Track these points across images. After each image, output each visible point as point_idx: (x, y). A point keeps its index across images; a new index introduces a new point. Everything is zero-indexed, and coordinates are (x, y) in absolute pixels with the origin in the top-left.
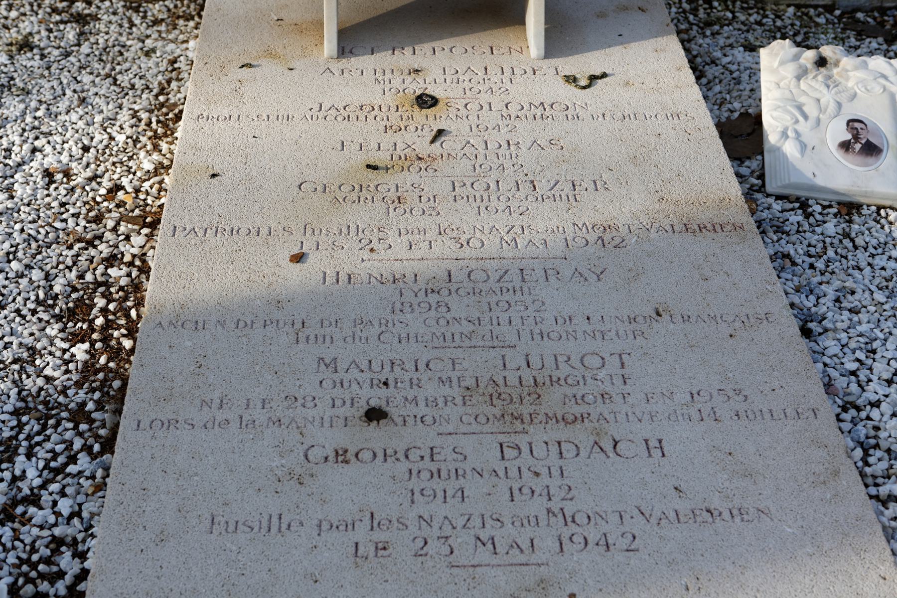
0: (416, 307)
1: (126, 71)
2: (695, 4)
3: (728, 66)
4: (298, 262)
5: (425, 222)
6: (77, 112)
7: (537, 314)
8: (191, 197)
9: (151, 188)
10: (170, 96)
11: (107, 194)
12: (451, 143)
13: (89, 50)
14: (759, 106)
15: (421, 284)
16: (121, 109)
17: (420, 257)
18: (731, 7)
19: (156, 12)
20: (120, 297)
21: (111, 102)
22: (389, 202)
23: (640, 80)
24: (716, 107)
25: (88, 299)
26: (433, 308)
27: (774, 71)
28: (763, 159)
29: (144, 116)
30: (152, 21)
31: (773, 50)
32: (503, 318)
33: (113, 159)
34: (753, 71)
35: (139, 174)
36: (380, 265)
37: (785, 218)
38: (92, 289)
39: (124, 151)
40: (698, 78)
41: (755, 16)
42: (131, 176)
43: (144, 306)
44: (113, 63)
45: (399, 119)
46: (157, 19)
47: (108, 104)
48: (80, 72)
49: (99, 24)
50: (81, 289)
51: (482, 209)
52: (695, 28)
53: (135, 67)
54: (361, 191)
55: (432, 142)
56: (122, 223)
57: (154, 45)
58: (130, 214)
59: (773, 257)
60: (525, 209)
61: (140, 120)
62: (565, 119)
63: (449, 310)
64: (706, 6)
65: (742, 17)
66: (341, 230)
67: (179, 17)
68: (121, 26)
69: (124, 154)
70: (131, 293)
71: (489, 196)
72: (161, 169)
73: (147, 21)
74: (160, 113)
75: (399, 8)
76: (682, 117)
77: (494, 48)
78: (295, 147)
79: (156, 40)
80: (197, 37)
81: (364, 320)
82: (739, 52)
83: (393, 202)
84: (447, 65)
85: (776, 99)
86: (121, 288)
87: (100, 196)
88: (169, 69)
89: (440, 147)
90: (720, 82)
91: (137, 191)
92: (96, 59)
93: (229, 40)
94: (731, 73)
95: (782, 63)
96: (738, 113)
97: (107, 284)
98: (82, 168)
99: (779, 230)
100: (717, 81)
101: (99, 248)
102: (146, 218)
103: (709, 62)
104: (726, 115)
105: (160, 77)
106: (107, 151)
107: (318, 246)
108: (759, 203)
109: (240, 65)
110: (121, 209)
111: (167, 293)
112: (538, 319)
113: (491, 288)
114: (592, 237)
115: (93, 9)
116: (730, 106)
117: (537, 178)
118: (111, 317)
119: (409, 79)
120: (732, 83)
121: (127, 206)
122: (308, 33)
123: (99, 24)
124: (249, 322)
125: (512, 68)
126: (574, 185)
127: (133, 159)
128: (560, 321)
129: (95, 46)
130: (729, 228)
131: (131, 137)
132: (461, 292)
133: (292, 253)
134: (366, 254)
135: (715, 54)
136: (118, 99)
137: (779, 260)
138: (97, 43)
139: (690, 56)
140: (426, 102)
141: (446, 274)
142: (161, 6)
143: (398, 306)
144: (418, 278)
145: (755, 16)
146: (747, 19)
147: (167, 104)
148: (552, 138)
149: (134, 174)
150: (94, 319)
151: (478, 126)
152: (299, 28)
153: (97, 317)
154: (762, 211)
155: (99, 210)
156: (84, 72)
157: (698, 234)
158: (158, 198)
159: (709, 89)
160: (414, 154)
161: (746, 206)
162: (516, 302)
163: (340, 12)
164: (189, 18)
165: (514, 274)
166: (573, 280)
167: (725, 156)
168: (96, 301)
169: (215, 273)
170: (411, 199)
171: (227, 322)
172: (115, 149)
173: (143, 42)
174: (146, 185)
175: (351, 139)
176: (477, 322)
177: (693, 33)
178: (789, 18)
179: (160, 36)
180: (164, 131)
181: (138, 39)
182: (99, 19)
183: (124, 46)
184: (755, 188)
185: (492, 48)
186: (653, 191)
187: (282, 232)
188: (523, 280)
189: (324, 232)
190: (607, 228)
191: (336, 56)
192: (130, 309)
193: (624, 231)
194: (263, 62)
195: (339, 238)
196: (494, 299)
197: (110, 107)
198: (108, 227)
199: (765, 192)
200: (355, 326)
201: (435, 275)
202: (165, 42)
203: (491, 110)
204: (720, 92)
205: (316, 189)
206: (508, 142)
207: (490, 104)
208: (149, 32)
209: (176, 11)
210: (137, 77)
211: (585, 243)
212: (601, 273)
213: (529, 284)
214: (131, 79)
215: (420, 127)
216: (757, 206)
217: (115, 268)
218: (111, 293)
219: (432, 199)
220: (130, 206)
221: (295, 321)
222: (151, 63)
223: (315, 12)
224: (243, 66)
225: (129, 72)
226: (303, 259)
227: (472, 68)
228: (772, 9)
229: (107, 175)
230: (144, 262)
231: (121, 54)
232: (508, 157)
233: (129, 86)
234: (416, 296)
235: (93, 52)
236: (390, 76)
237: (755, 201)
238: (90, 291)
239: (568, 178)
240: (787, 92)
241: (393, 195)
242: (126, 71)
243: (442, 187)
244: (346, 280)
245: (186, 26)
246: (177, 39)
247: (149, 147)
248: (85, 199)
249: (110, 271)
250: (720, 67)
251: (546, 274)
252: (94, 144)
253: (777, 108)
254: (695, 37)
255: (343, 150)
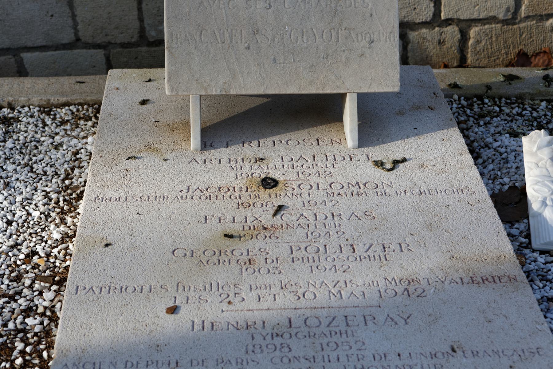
0: (264, 348)
1: (40, 161)
2: (471, 101)
3: (498, 149)
4: (172, 313)
5: (270, 279)
6: (3, 194)
7: (359, 352)
8: (90, 262)
9: (59, 253)
10: (73, 180)
11: (25, 258)
12: (288, 216)
13: (13, 145)
14: (523, 180)
15: (269, 330)
16: (36, 191)
17: (267, 308)
18: (498, 103)
19: (63, 115)
20: (35, 342)
21: (29, 186)
22: (242, 263)
23: (432, 163)
24: (491, 181)
25: (10, 343)
26: (278, 349)
27: (533, 154)
28: (529, 222)
29: (54, 196)
30: (60, 122)
31: (532, 139)
32: (333, 355)
33: (30, 231)
34: (517, 152)
35: (49, 242)
36: (236, 314)
37: (548, 269)
38: (13, 335)
39: (38, 224)
40: (475, 158)
41: (517, 109)
42: (43, 244)
43: (53, 348)
44: (30, 154)
45: (248, 198)
46: (63, 120)
47: (26, 187)
48: (5, 162)
49: (20, 125)
50: (5, 335)
51: (314, 268)
52: (471, 119)
53: (47, 158)
54: (220, 255)
55: (275, 215)
56: (36, 282)
57: (61, 140)
58: (43, 274)
59: (541, 301)
60: (347, 267)
61: (50, 200)
62: (376, 195)
63: (290, 350)
64: (479, 102)
65: (507, 111)
66: (205, 287)
67: (80, 118)
68: (36, 126)
69: (38, 226)
70: (43, 338)
71: (319, 258)
72: (66, 238)
73: (56, 122)
74: (66, 194)
75: (247, 111)
76: (465, 191)
77: (320, 141)
78: (169, 221)
79: (63, 136)
80: (94, 133)
81: (224, 359)
82: (506, 138)
83: (245, 263)
84: (285, 154)
85: (536, 176)
86: (36, 334)
87: (20, 260)
88: (73, 159)
89: (280, 219)
90: (493, 161)
91: (48, 255)
92: (17, 152)
93: (119, 138)
94: (501, 154)
95: (539, 148)
96: (508, 186)
97: (25, 331)
98: (6, 238)
99: (543, 278)
100: (490, 160)
101: (19, 301)
102: (55, 277)
103: (484, 146)
104: (498, 187)
105: (66, 166)
106: (25, 224)
107: (188, 300)
108: (527, 257)
109: (127, 158)
110: (36, 271)
111: (71, 340)
112: (360, 357)
113: (323, 332)
114: (400, 289)
115: (16, 113)
116: (501, 180)
117: (356, 242)
118: (28, 358)
119: (255, 166)
120: (501, 162)
121: (41, 268)
122: (178, 131)
123: (20, 125)
124: (135, 363)
125: (334, 156)
126: (384, 248)
127: (45, 230)
128: (377, 357)
129: (16, 142)
130: (505, 279)
131: (44, 213)
132: (299, 335)
133: (168, 306)
134: (225, 306)
135: (487, 139)
136: (34, 183)
137: (545, 303)
138: (18, 140)
139: (469, 142)
140: (269, 184)
141: (287, 321)
142: (67, 110)
143: (250, 348)
144: (265, 324)
145: (517, 109)
146: (511, 112)
147: (71, 187)
148: (366, 210)
149: (46, 242)
150: (15, 360)
151: (309, 202)
152: (171, 128)
153: (17, 358)
154: (530, 264)
155: (19, 271)
156: (8, 162)
157: (482, 285)
158: (64, 261)
159: (485, 167)
160: (260, 225)
161: (518, 261)
162: (342, 343)
163: (202, 115)
164: (87, 119)
165: (340, 320)
166: (386, 324)
167: (500, 222)
168: (16, 344)
169: (108, 323)
170: (259, 261)
171: (118, 363)
172: (32, 222)
173: (53, 138)
174: (55, 251)
175: (212, 214)
176: (312, 360)
177: (471, 123)
178: (543, 110)
179: (66, 133)
180: (69, 208)
181: (50, 136)
182: (20, 121)
183: (38, 142)
184: (523, 245)
185: (318, 141)
186: (445, 251)
187: (160, 289)
188: (348, 325)
189: (192, 288)
190: (411, 281)
191: (199, 147)
192: (43, 351)
193: (424, 283)
194: (144, 154)
195: (204, 294)
196: (325, 341)
197: (28, 189)
198: (26, 285)
199: (531, 248)
200: (217, 365)
201: (279, 322)
202: (70, 138)
203: (318, 189)
204: (493, 170)
205: (186, 254)
206: (333, 214)
207: (318, 184)
208: (57, 130)
209: (78, 114)
210: (49, 165)
211: (394, 293)
212: (408, 318)
213: (352, 328)
214: (44, 167)
215: (264, 204)
216: (526, 259)
217: (31, 318)
218: (28, 338)
219: (275, 261)
220: (42, 268)
221: (171, 362)
222: (59, 155)
223: (183, 115)
224: (129, 158)
225: (42, 162)
226: (176, 311)
227: (303, 156)
228: (529, 104)
229: (25, 244)
230: (53, 312)
231: (37, 148)
232: (333, 226)
233: (42, 173)
234: (264, 339)
235: (15, 147)
236: (242, 164)
237: (524, 255)
238: (12, 336)
239: (380, 242)
240: (544, 170)
241: (245, 258)
242: (40, 161)
243: (282, 251)
244: (210, 327)
245: (86, 125)
246: (79, 135)
247: (57, 221)
248: (8, 263)
249: (27, 320)
250: (492, 150)
251: (365, 320)
252: (15, 219)
253: (537, 183)
254: (472, 126)
255: (206, 222)
